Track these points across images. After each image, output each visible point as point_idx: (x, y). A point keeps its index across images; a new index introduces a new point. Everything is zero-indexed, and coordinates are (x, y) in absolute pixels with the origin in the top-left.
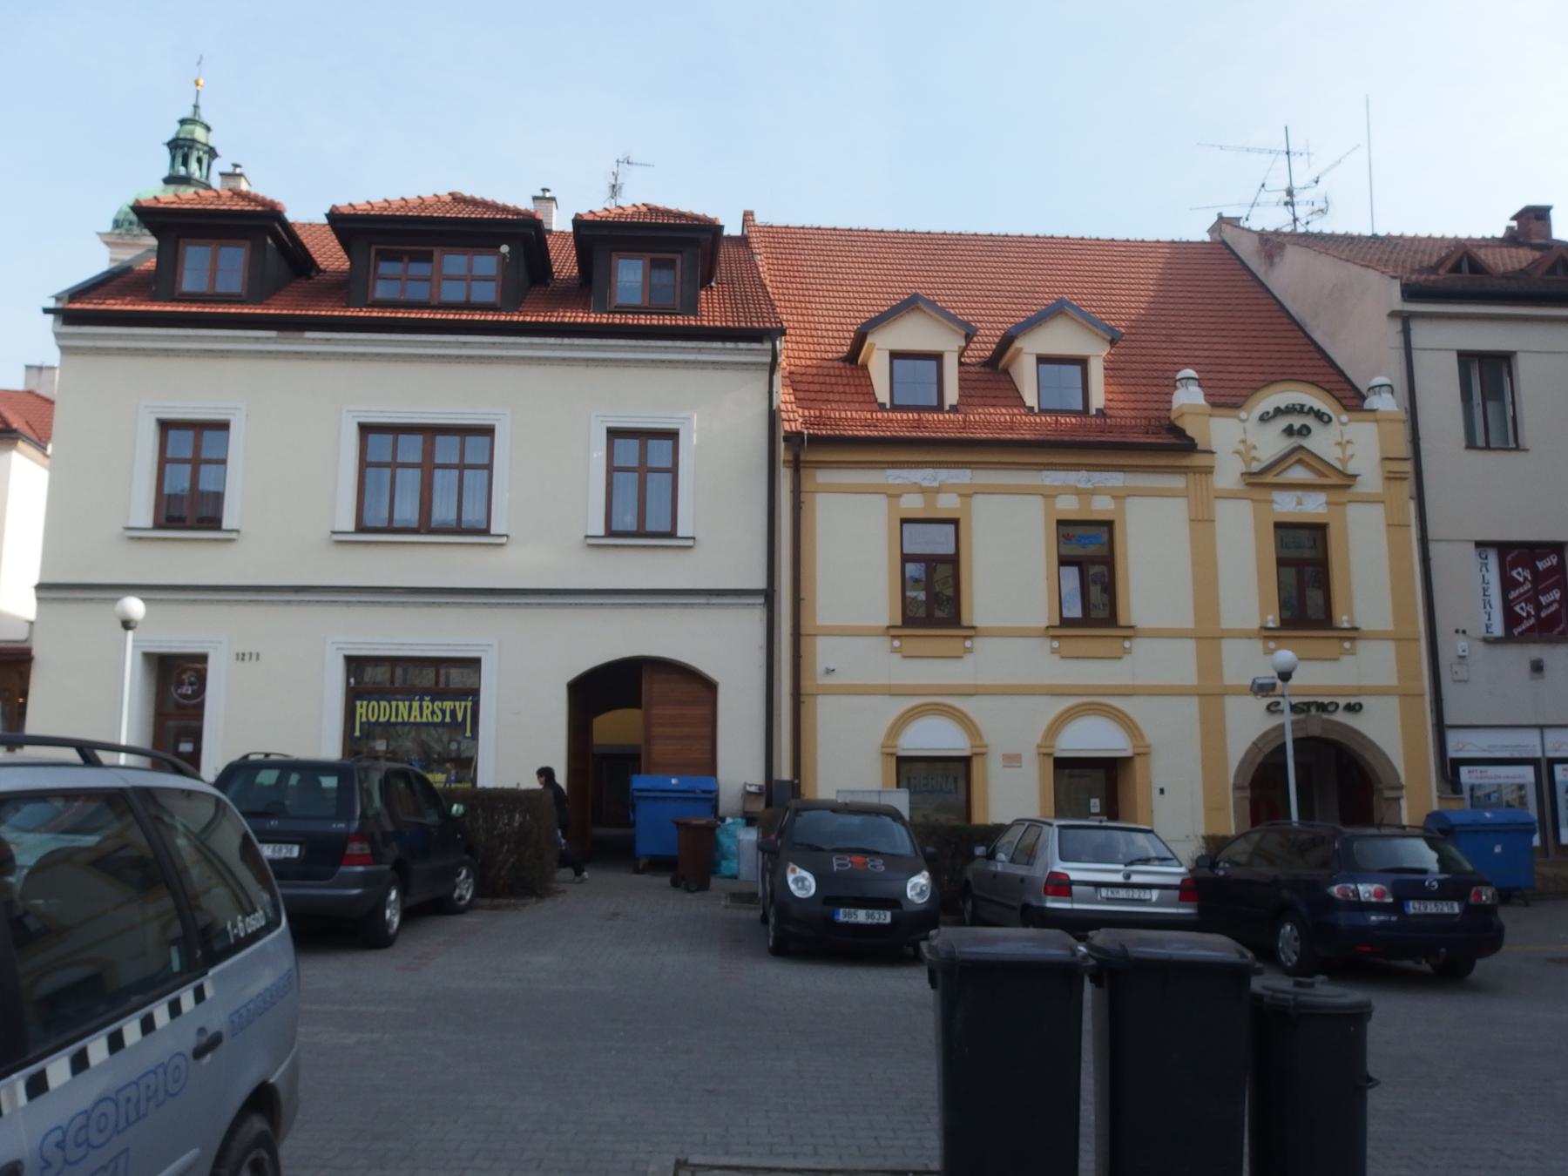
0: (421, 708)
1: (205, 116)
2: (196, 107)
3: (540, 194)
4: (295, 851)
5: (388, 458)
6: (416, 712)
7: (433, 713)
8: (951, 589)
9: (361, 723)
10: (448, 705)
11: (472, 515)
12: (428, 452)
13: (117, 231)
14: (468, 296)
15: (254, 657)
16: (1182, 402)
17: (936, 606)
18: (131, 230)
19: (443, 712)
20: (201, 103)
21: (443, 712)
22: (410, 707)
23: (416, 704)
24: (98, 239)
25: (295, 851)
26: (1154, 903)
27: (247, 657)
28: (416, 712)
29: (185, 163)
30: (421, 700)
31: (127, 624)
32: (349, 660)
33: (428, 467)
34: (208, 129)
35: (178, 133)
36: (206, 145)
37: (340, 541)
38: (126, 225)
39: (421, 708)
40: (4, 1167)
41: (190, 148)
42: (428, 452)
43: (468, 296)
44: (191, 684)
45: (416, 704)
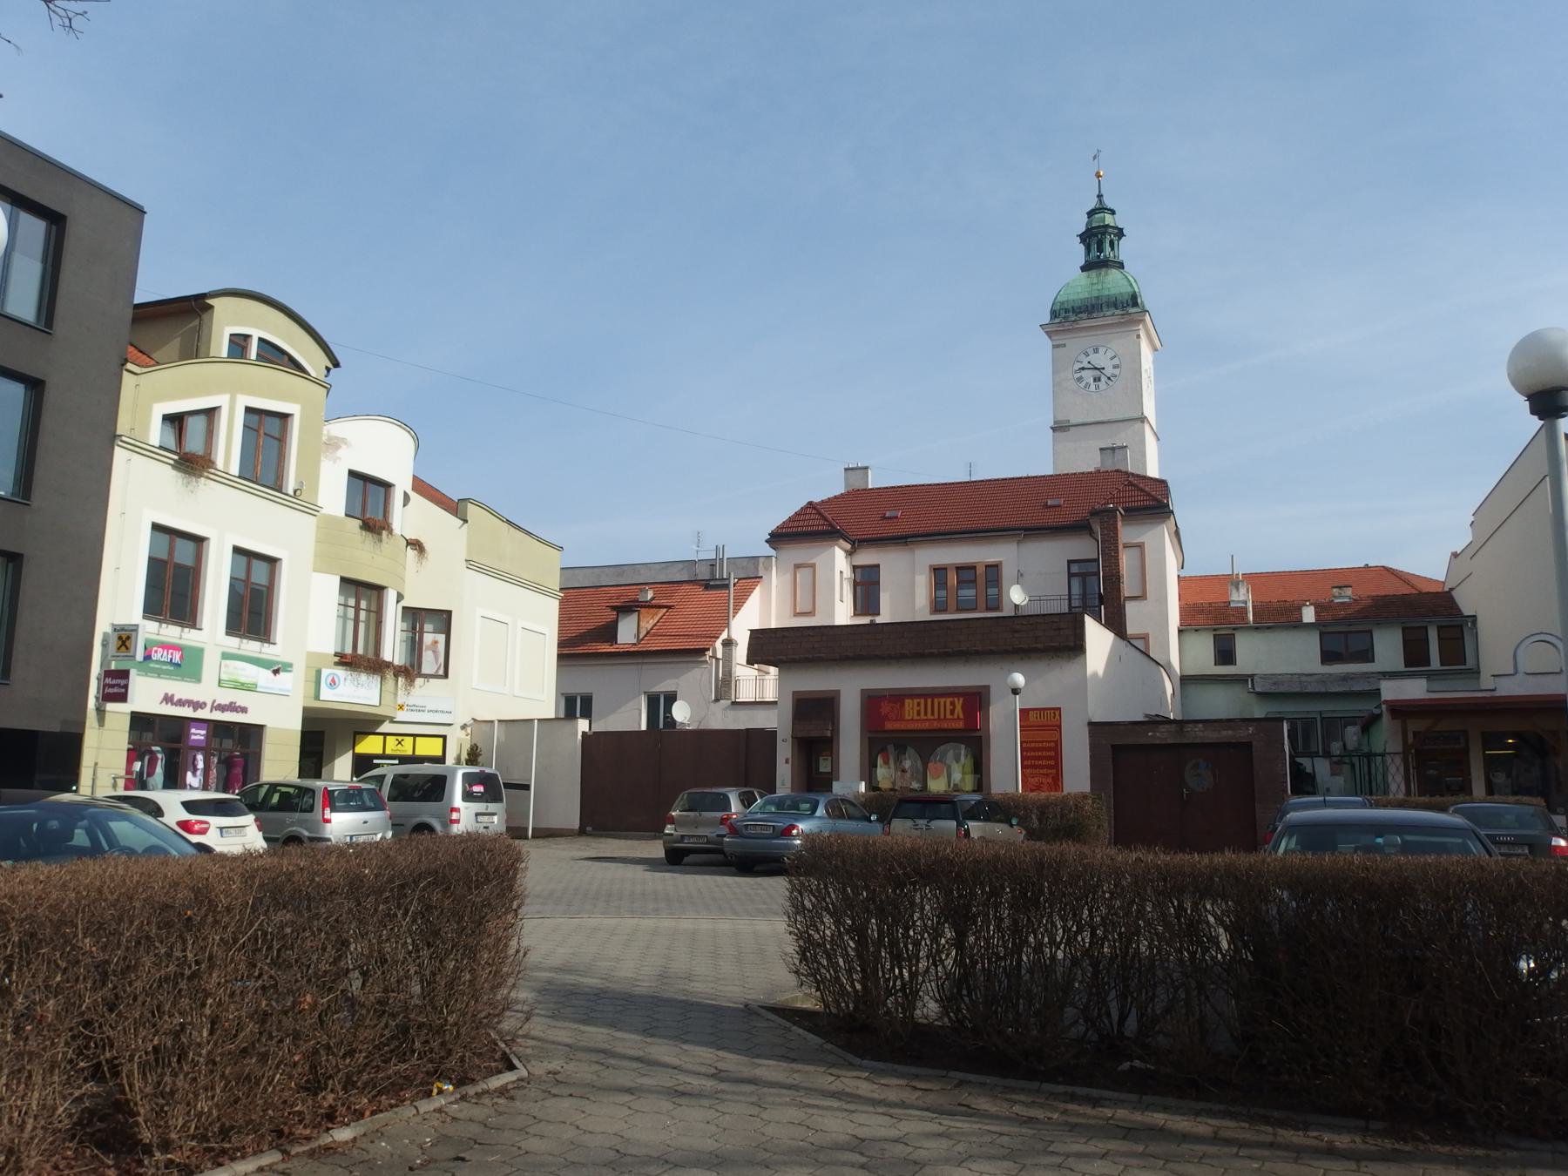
1: (1109, 203)
2: (1100, 196)
4: (1103, 607)
8: (1077, 571)
13: (1057, 321)
16: (792, 980)
17: (1524, 957)
20: (1102, 192)
25: (1103, 607)
26: (1140, 1154)
29: (1100, 249)
34: (1113, 212)
36: (1117, 228)
41: (1104, 234)
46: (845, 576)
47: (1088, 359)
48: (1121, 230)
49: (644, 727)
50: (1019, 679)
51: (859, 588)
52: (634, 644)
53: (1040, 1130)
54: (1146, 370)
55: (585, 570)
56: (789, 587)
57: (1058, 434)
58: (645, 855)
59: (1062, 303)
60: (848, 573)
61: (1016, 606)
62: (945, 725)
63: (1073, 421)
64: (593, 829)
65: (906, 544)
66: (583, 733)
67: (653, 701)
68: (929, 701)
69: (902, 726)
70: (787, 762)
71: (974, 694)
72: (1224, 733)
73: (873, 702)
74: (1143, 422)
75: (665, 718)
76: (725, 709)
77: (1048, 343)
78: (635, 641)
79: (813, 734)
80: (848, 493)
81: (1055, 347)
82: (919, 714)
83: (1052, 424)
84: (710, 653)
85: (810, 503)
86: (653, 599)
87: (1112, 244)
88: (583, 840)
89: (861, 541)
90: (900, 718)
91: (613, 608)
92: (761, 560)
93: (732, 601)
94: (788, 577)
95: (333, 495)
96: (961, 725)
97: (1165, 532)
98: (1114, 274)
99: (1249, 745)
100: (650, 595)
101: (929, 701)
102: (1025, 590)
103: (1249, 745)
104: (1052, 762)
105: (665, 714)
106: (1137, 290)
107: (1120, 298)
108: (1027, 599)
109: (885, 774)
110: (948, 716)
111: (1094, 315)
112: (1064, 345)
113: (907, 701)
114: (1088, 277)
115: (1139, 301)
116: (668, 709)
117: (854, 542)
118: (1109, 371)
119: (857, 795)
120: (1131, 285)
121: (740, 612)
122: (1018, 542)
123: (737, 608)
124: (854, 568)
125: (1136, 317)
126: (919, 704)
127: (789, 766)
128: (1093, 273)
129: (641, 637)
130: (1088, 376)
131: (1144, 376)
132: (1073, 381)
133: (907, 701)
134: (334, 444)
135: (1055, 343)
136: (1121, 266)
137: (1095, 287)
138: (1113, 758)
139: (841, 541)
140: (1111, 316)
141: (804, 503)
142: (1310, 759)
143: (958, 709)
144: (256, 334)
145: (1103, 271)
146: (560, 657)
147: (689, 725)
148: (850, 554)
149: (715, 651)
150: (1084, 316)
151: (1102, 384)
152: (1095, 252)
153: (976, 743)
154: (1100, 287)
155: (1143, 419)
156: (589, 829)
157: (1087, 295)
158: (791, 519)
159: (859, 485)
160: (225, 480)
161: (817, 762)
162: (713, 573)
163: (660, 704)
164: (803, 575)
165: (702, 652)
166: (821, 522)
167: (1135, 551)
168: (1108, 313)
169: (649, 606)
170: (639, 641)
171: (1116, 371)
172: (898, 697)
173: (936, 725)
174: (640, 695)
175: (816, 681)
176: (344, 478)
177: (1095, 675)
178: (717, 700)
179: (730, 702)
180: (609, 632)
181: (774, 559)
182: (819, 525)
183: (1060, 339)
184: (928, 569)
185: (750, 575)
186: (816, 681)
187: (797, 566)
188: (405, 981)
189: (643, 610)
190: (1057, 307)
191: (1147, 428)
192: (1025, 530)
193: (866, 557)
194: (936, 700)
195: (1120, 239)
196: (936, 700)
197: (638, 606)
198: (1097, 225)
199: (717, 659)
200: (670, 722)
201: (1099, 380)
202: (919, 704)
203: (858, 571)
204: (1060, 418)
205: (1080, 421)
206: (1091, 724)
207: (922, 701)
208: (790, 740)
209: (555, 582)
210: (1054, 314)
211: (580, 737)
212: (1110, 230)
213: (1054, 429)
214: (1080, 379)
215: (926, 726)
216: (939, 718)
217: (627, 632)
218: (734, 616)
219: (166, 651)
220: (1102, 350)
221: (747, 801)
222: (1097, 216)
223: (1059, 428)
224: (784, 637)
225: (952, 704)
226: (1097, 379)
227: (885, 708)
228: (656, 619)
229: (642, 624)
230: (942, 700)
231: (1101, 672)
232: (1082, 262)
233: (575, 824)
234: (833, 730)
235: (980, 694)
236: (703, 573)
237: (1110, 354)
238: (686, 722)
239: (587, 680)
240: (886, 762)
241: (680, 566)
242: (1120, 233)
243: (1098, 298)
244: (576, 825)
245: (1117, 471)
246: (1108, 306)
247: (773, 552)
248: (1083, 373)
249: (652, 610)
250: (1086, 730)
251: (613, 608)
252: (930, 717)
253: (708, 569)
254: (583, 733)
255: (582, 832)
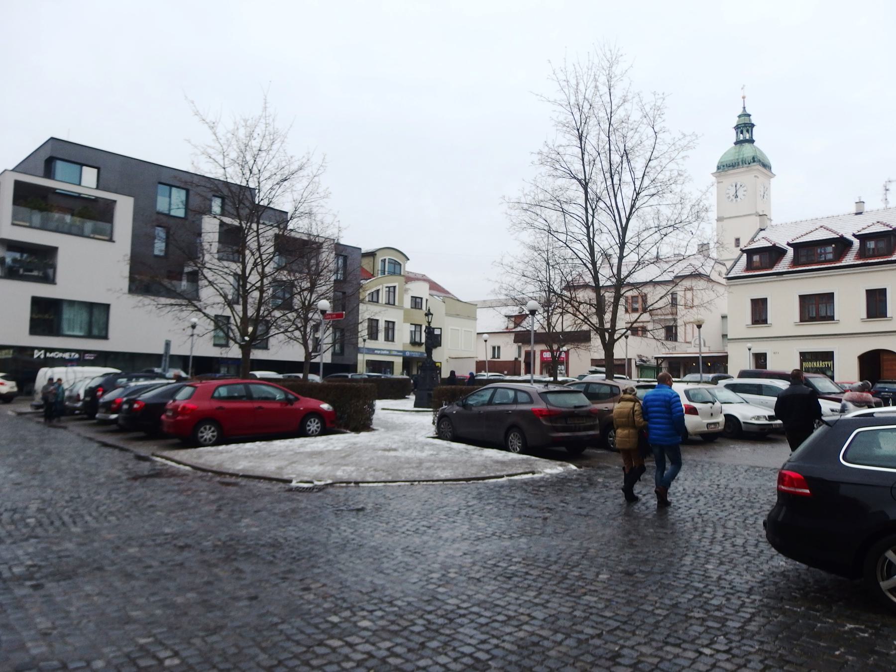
1: (748, 111)
2: (744, 108)
95: (407, 303)
134: (406, 290)
142: (331, 342)
144: (387, 258)
160: (382, 305)
176: (410, 298)
188: (227, 162)
205: (728, 216)
219: (651, 415)
232: (735, 140)
243: (738, 159)
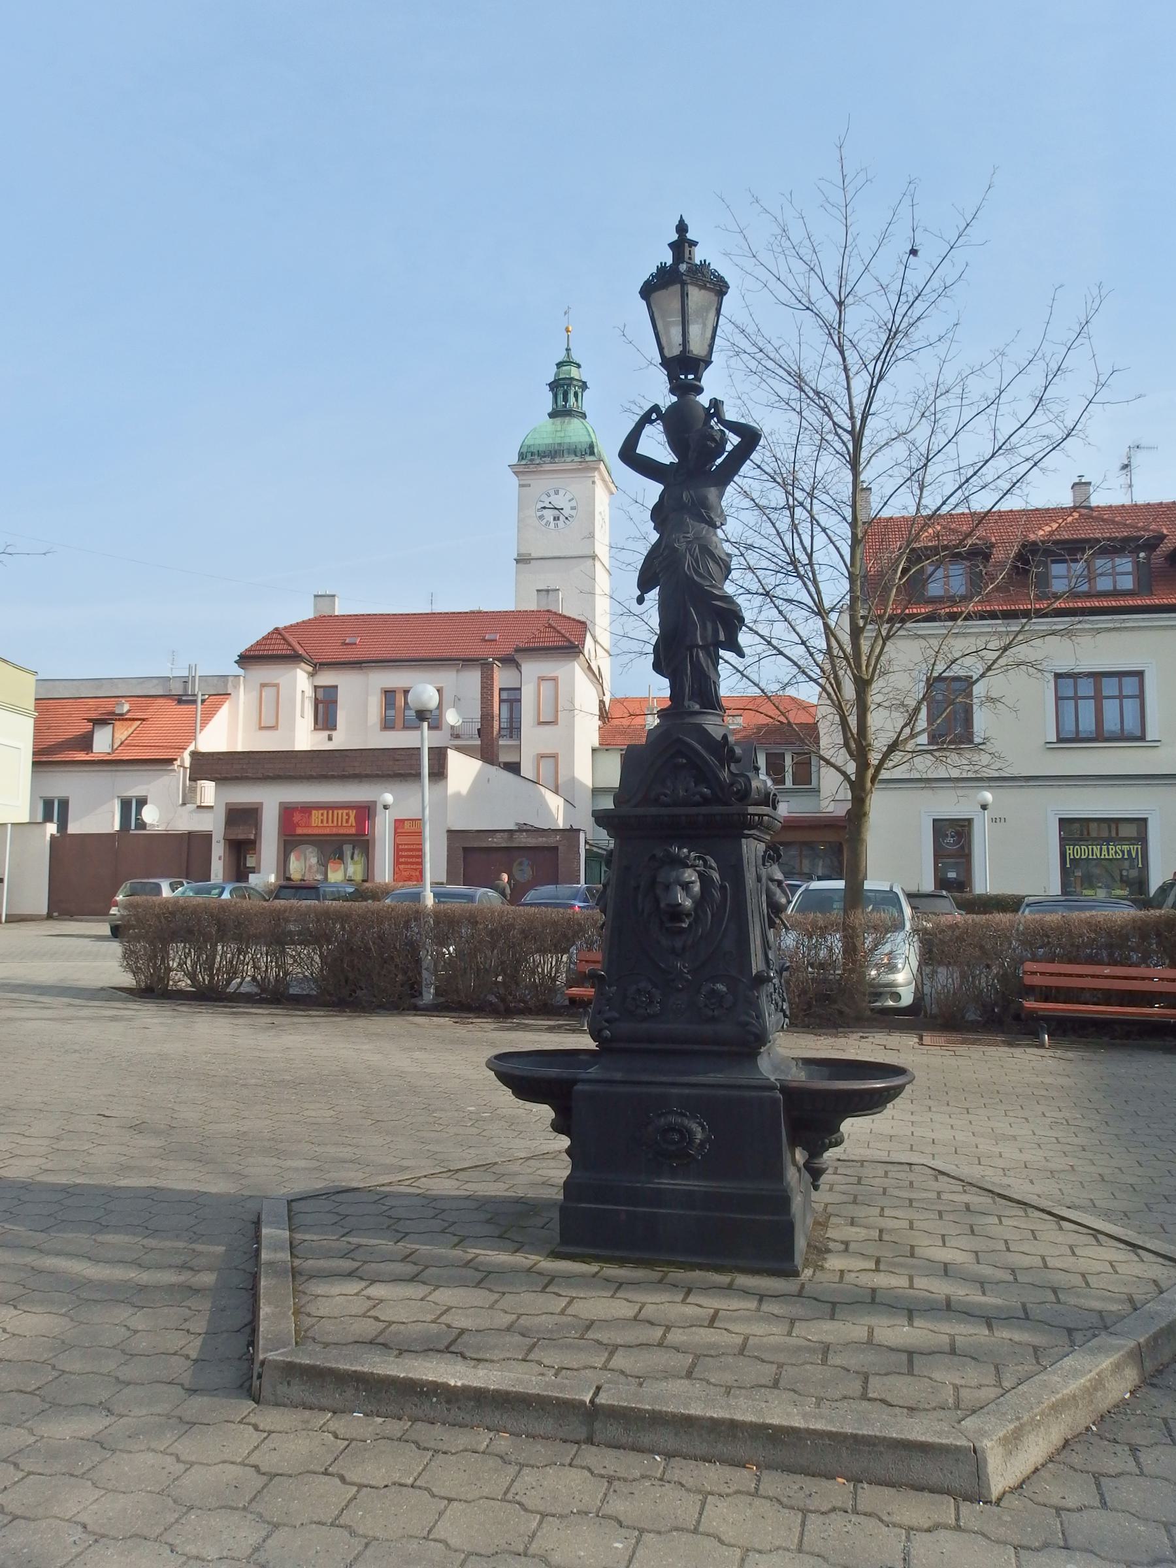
0: (1108, 849)
1: (576, 357)
2: (568, 350)
3: (1077, 480)
5: (1071, 694)
6: (1105, 852)
7: (1116, 852)
9: (1070, 859)
10: (1126, 848)
11: (1131, 725)
12: (1098, 689)
13: (524, 462)
14: (1115, 586)
15: (1003, 820)
18: (533, 460)
19: (1123, 852)
20: (571, 346)
21: (1123, 852)
22: (1101, 849)
23: (1104, 847)
24: (509, 470)
27: (998, 820)
28: (1105, 852)
29: (566, 399)
30: (1108, 844)
31: (984, 807)
32: (1061, 820)
33: (1098, 698)
34: (579, 366)
35: (557, 374)
36: (581, 381)
37: (1049, 747)
38: (529, 457)
39: (1108, 849)
40: (1168, 1050)
41: (569, 385)
42: (1098, 689)
43: (1115, 586)
44: (952, 837)
45: (1104, 847)
46: (307, 694)
47: (550, 499)
48: (585, 383)
49: (117, 827)
50: (388, 798)
51: (321, 706)
52: (109, 754)
53: (761, 1298)
54: (600, 513)
55: (64, 682)
56: (256, 703)
57: (520, 565)
58: (88, 933)
59: (529, 446)
60: (309, 692)
61: (452, 727)
62: (342, 831)
63: (534, 555)
64: (60, 915)
65: (361, 668)
66: (52, 835)
67: (126, 804)
68: (330, 812)
69: (309, 831)
70: (220, 859)
71: (365, 807)
72: (540, 839)
73: (288, 813)
74: (594, 559)
75: (137, 819)
76: (191, 812)
77: (514, 481)
78: (109, 750)
79: (241, 837)
80: (316, 619)
81: (521, 486)
82: (322, 822)
83: (516, 556)
84: (178, 763)
85: (276, 629)
86: (129, 711)
87: (576, 395)
88: (51, 923)
89: (321, 664)
90: (308, 826)
91: (89, 720)
92: (230, 679)
93: (199, 718)
94: (255, 694)
96: (353, 831)
97: (577, 670)
98: (576, 423)
99: (556, 848)
100: (126, 708)
101: (330, 812)
102: (459, 712)
103: (556, 848)
104: (401, 860)
105: (136, 815)
106: (594, 440)
107: (579, 447)
108: (461, 721)
109: (296, 868)
110: (344, 824)
111: (556, 460)
112: (530, 486)
113: (314, 812)
114: (553, 424)
115: (596, 450)
116: (139, 812)
117: (316, 665)
118: (566, 512)
119: (269, 885)
120: (589, 435)
121: (206, 729)
122: (458, 671)
123: (205, 723)
124: (316, 687)
125: (592, 465)
126: (322, 815)
127: (221, 863)
128: (558, 420)
129: (115, 747)
130: (549, 515)
131: (597, 517)
132: (535, 519)
133: (314, 812)
135: (522, 483)
136: (584, 416)
137: (559, 434)
138: (464, 858)
139: (303, 664)
140: (570, 462)
141: (270, 629)
143: (352, 820)
145: (567, 419)
146: (35, 764)
147: (158, 826)
148: (312, 675)
149: (183, 761)
150: (548, 460)
151: (561, 523)
152: (561, 403)
153: (363, 844)
154: (563, 435)
155: (594, 557)
156: (55, 914)
157: (551, 441)
158: (258, 643)
159: (327, 612)
161: (245, 859)
162: (185, 689)
163: (130, 807)
164: (268, 693)
165: (171, 761)
166: (286, 647)
167: (551, 683)
168: (569, 459)
169: (121, 718)
170: (114, 750)
171: (573, 513)
172: (307, 809)
173: (334, 831)
174: (113, 799)
175: (244, 795)
177: (458, 795)
178: (184, 804)
179: (195, 806)
180: (86, 742)
181: (242, 678)
182: (281, 649)
183: (527, 479)
184: (379, 691)
185: (220, 693)
186: (244, 795)
187: (263, 685)
189: (117, 723)
190: (524, 450)
191: (598, 564)
192: (464, 660)
193: (327, 678)
194: (336, 812)
195: (583, 390)
196: (336, 812)
197: (112, 719)
198: (564, 376)
199: (185, 768)
200: (141, 825)
201: (558, 519)
202: (322, 815)
203: (320, 691)
204: (523, 551)
206: (449, 831)
207: (325, 812)
208: (222, 841)
209: (30, 704)
210: (522, 456)
211: (48, 838)
212: (575, 383)
213: (517, 561)
214: (541, 517)
215: (327, 831)
216: (337, 826)
217: (103, 742)
218: (201, 730)
220: (561, 492)
221: (173, 888)
222: (564, 368)
223: (522, 560)
224: (220, 759)
225: (348, 814)
226: (556, 519)
227: (297, 817)
228: (131, 730)
229: (116, 735)
230: (340, 812)
231: (464, 790)
232: (550, 410)
233: (44, 910)
234: (256, 834)
235: (369, 808)
236: (177, 689)
237: (568, 496)
238: (155, 823)
239: (62, 785)
240: (298, 859)
241: (155, 681)
242: (584, 386)
243: (560, 444)
244: (44, 911)
245: (548, 611)
246: (569, 453)
247: (241, 672)
248: (545, 512)
249: (125, 723)
250: (445, 836)
251: (89, 720)
252: (330, 824)
253: (182, 685)
254: (52, 835)
255: (49, 917)
